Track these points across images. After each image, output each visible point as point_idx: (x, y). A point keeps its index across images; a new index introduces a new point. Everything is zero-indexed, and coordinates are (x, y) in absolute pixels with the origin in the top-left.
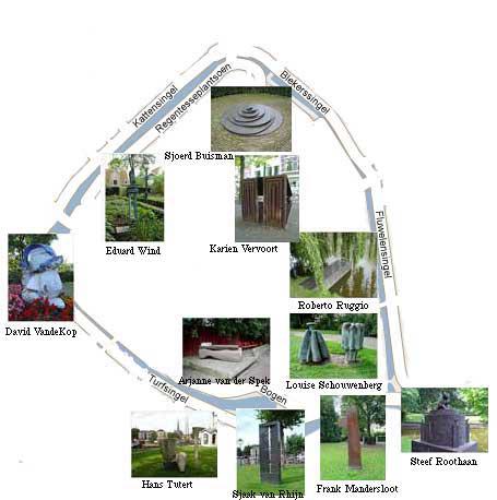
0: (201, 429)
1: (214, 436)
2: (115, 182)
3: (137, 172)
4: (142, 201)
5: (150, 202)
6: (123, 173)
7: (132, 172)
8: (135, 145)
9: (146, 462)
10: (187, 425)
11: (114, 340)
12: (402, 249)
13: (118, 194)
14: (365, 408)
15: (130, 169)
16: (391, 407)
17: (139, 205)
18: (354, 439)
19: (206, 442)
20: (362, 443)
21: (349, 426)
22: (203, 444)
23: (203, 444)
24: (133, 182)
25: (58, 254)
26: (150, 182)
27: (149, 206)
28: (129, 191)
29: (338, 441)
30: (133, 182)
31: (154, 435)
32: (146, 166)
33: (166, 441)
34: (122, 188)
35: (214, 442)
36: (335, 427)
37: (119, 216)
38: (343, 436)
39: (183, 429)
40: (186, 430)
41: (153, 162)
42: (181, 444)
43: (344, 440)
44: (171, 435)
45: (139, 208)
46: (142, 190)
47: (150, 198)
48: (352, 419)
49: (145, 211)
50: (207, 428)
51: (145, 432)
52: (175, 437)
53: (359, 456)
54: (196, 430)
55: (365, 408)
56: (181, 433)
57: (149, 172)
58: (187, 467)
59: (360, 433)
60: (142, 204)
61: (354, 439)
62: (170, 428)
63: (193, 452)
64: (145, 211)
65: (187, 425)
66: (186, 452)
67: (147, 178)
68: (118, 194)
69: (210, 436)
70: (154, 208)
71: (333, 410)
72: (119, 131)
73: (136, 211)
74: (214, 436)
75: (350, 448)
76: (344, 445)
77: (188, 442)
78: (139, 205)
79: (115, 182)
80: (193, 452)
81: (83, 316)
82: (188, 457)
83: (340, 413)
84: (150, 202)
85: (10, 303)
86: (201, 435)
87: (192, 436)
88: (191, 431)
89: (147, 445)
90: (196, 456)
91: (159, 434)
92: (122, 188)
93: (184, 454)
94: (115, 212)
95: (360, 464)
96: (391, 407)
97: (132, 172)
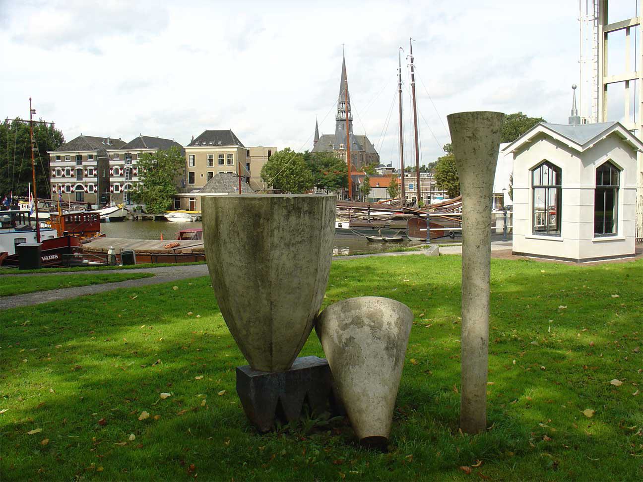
0: (515, 128)
1: (607, 177)
8: (319, 134)
9: (107, 368)
10: (408, 92)
11: (413, 73)
19: (549, 223)
22: (525, 240)
23: (525, 240)
31: (163, 170)
33: (254, 218)
35: (604, 222)
39: (375, 124)
40: (404, 134)
42: (366, 235)
44: (289, 171)
50: (551, 111)
51: (102, 148)
52: (324, 176)
54: (479, 136)
56: (368, 157)
58: (406, 403)
62: (285, 125)
63: (457, 297)
65: (408, 92)
66: (405, 295)
69: (579, 184)
74: (607, 177)
77: (416, 224)
80: (457, 297)
81: (506, 146)
82: (417, 330)
86: (512, 170)
87: (449, 176)
88: (436, 142)
89: (112, 241)
90: (478, 320)
91: (199, 161)
93: (385, 311)
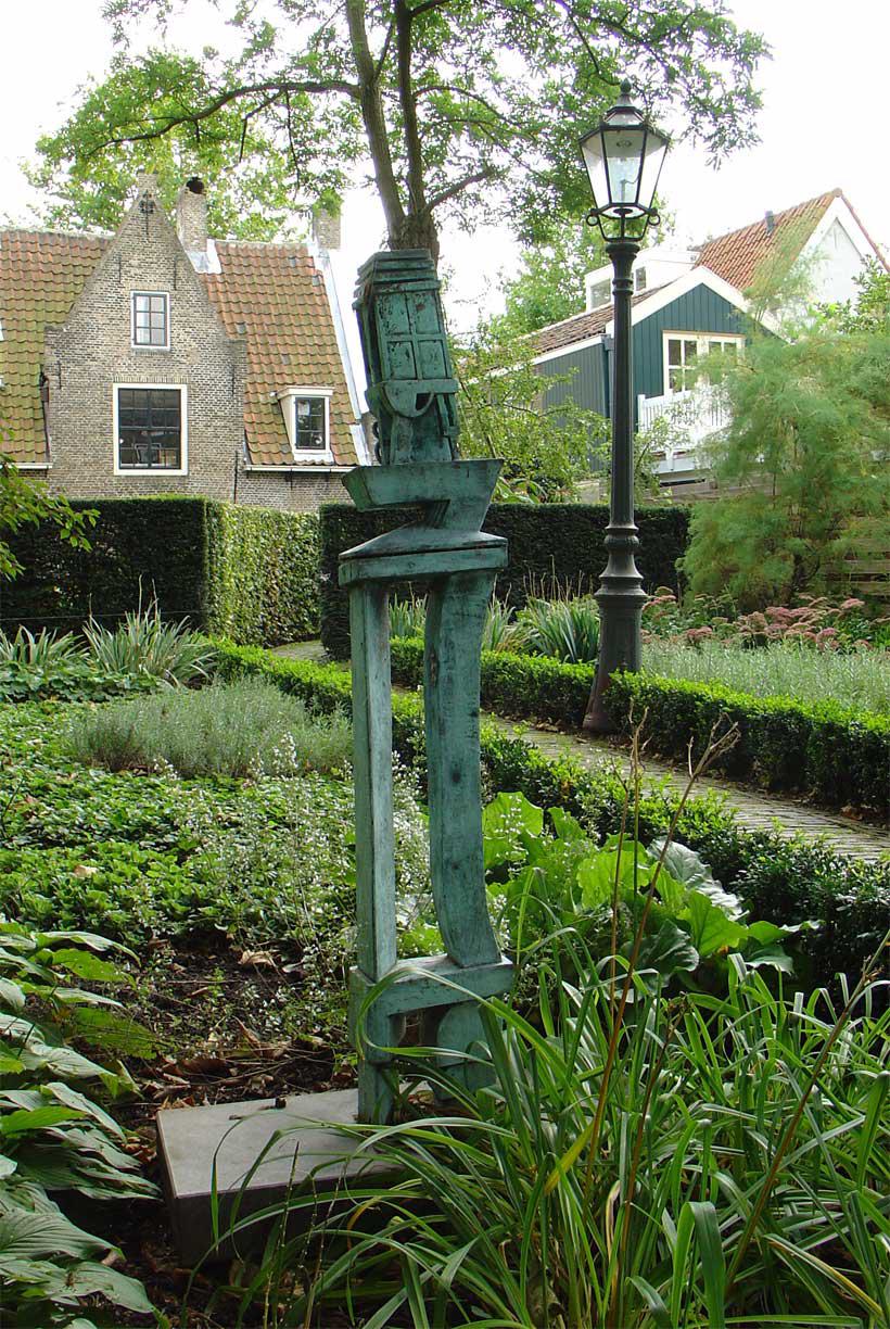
2: (150, 424)
3: (481, 270)
4: (559, 707)
5: (677, 730)
6: (268, 291)
7: (403, 276)
12: (757, 149)
13: (185, 602)
15: (365, 228)
16: (623, 198)
17: (508, 775)
24: (416, 414)
26: (685, 423)
27: (661, 788)
28: (358, 561)
30: (416, 414)
32: (606, 179)
34: (258, 520)
37: (203, 942)
41: (724, 120)
45: (511, 819)
46: (551, 546)
47: (678, 661)
49: (600, 869)
57: (666, 272)
60: (553, 752)
64: (600, 869)
67: (627, 367)
68: (185, 602)
70: (750, 816)
73: (458, 870)
78: (508, 775)
79: (150, 424)
84: (677, 730)
85: (338, 229)
92: (258, 520)
94: (149, 884)
96: (623, 198)
97: (403, 276)
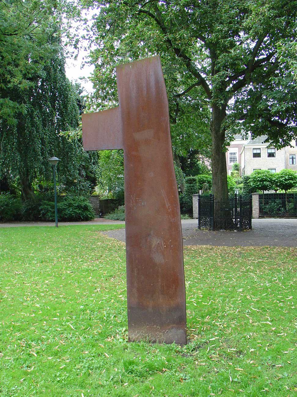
14: (202, 62)
18: (152, 204)
20: (190, 223)
21: (131, 153)
25: (281, 149)
29: (80, 216)
36: (65, 150)
38: (102, 192)
40: (279, 150)
43: (107, 208)
48: (142, 114)
53: (174, 282)
55: (202, 62)
59: (181, 179)
61: (152, 204)
71: (54, 69)
72: (293, 158)
75: (135, 242)
76: (107, 238)
83: (88, 89)
95: (181, 321)
